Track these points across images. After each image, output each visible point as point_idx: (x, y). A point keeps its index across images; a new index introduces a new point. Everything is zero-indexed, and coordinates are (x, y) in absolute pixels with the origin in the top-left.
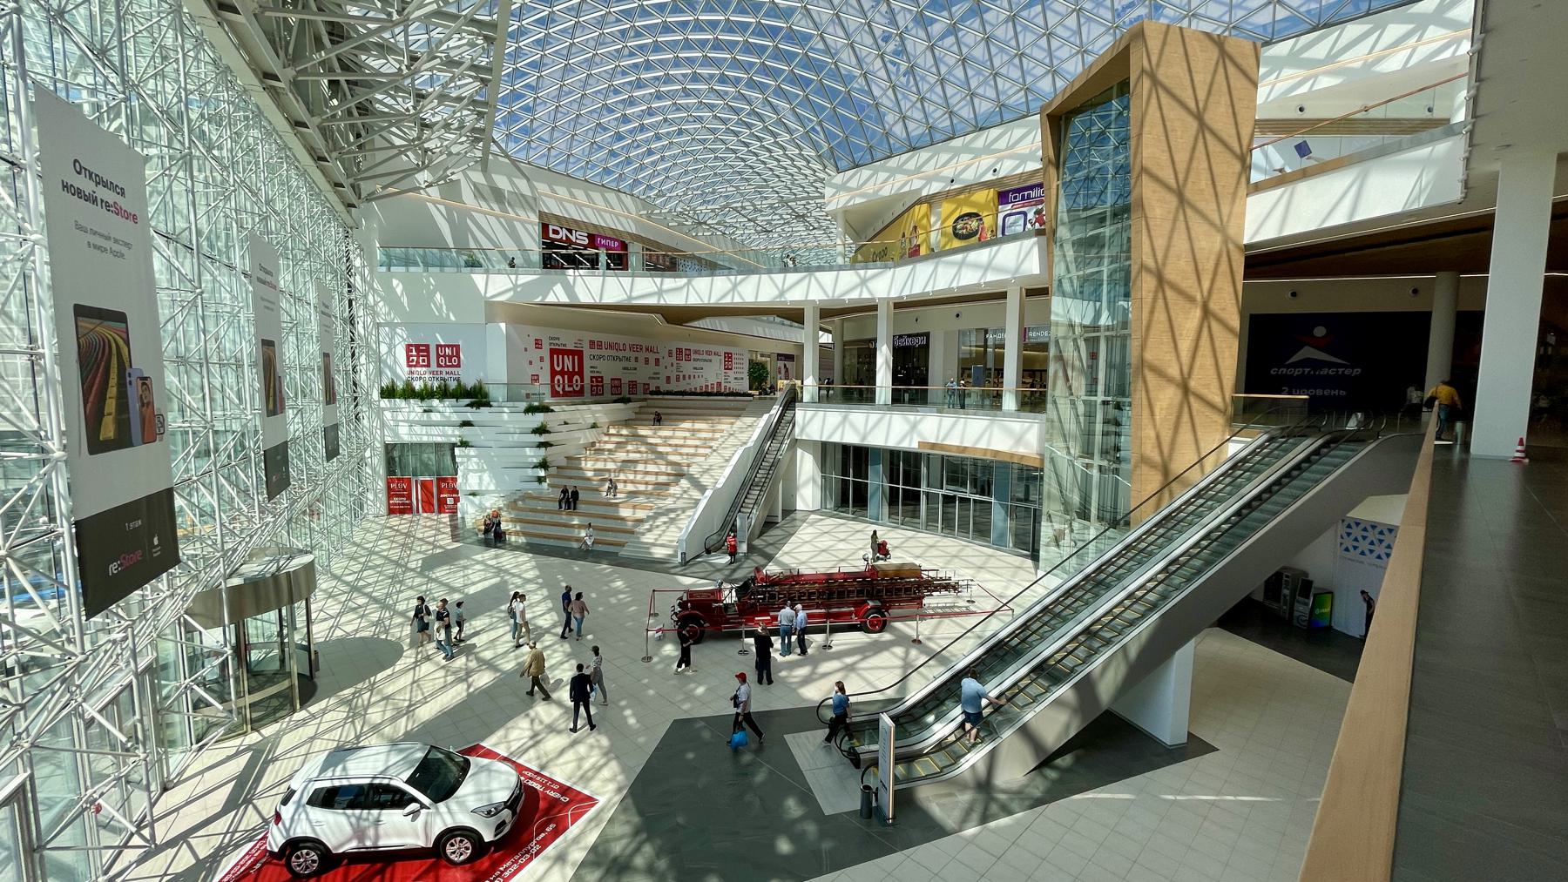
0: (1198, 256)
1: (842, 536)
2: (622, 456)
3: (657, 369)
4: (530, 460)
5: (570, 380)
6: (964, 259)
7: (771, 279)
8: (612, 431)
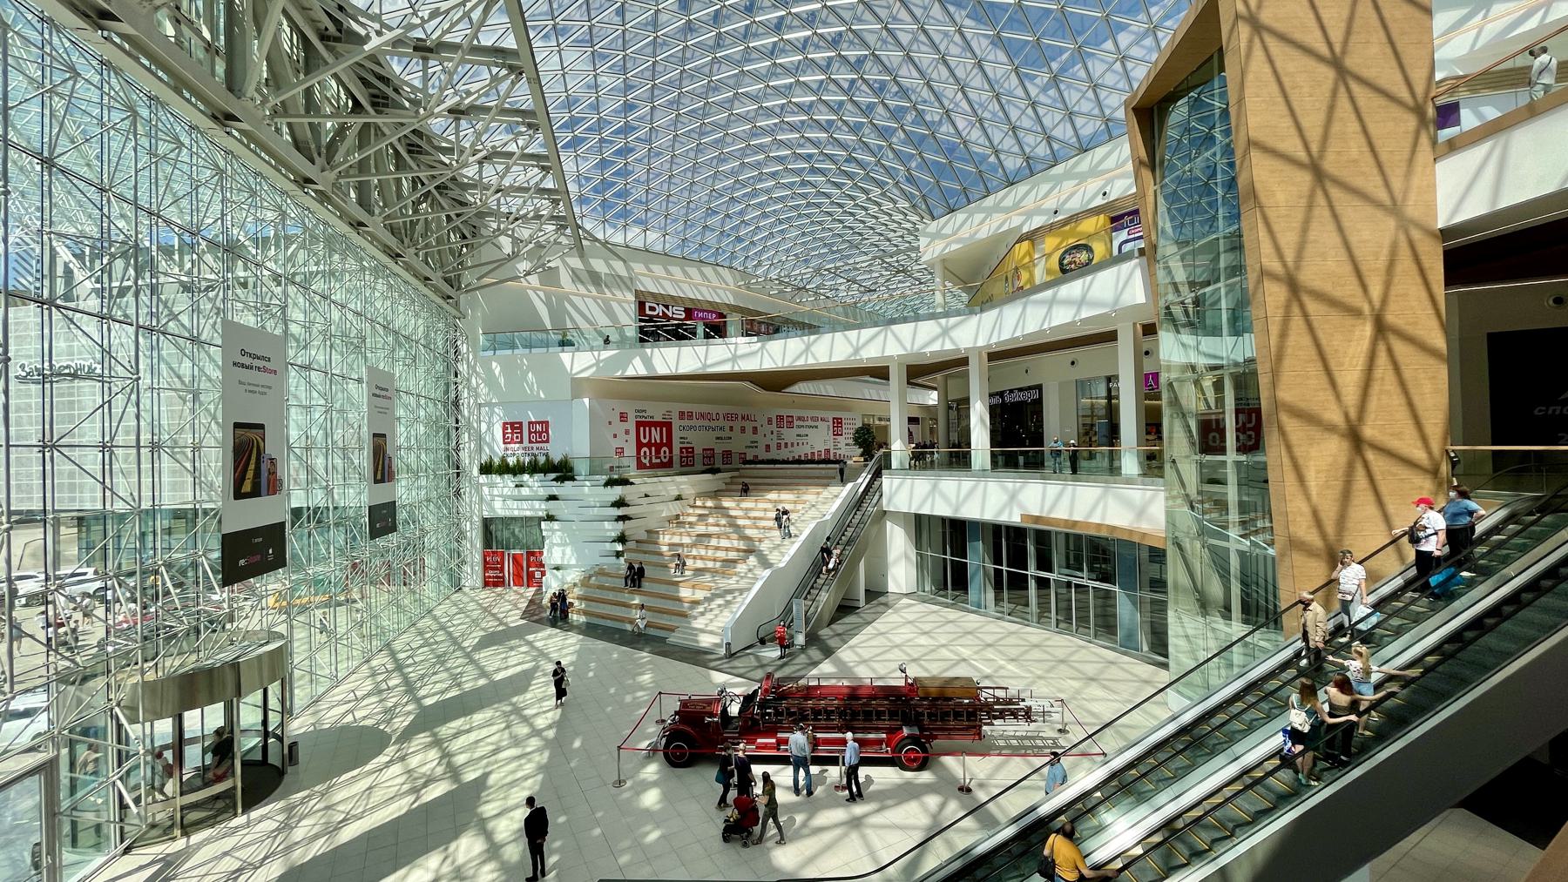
0: (1357, 253)
1: (927, 627)
2: (701, 529)
3: (755, 438)
4: (608, 534)
5: (658, 452)
6: (1055, 295)
7: (845, 336)
8: (699, 503)
